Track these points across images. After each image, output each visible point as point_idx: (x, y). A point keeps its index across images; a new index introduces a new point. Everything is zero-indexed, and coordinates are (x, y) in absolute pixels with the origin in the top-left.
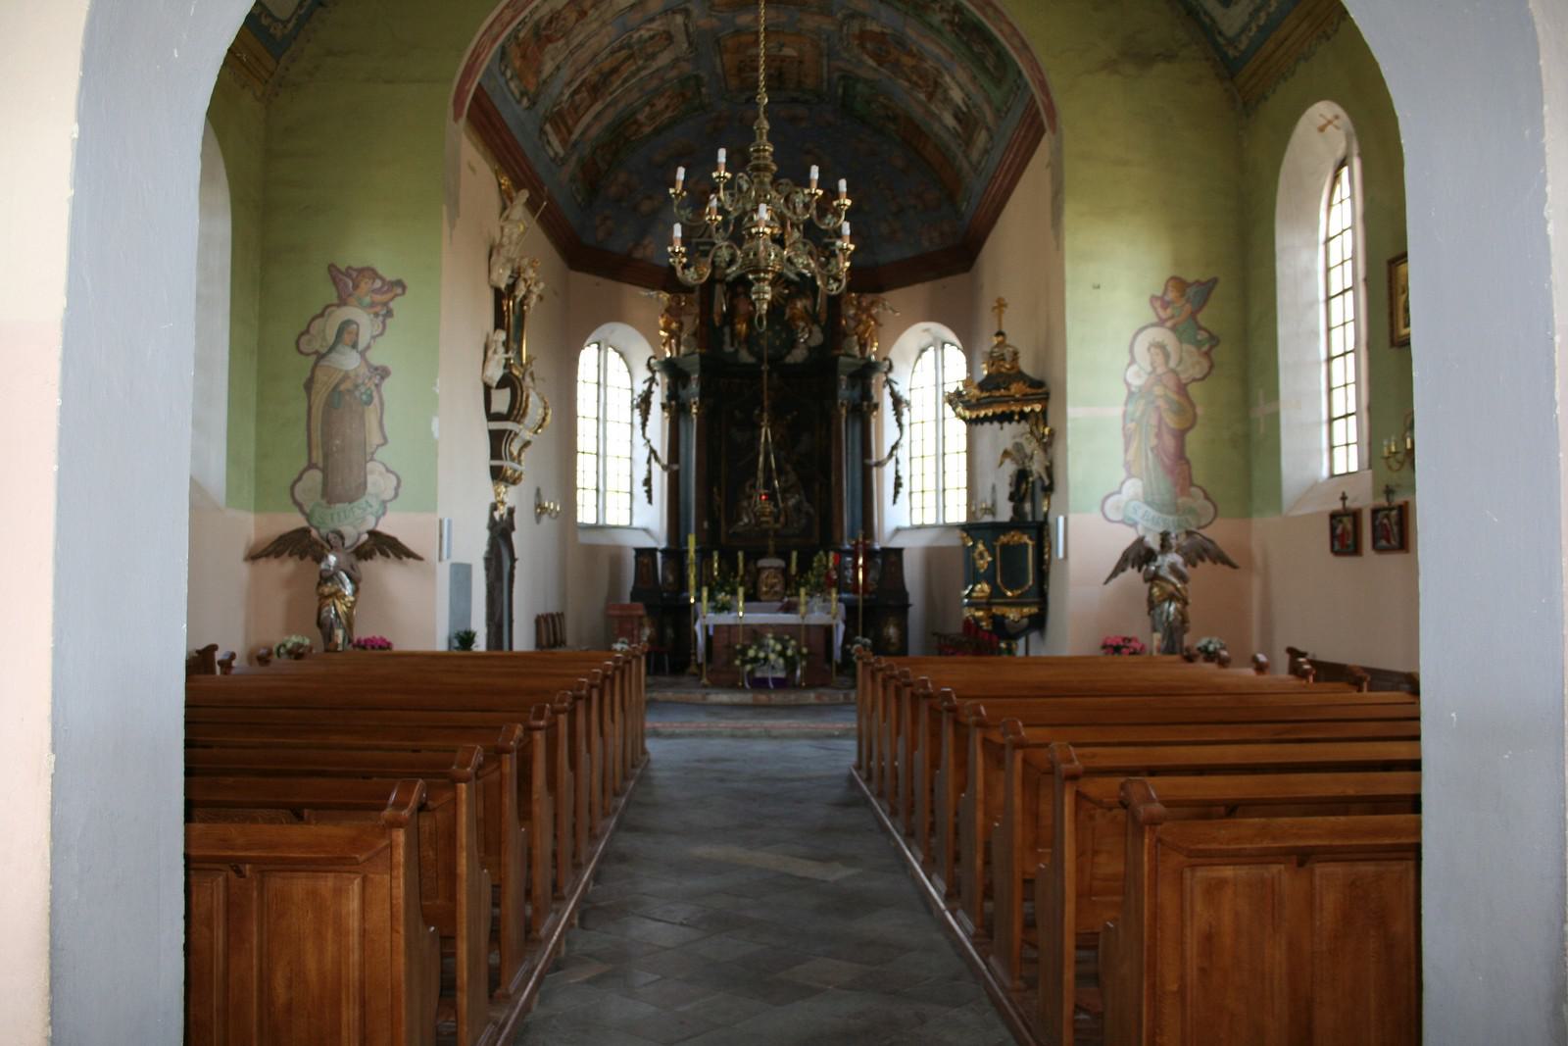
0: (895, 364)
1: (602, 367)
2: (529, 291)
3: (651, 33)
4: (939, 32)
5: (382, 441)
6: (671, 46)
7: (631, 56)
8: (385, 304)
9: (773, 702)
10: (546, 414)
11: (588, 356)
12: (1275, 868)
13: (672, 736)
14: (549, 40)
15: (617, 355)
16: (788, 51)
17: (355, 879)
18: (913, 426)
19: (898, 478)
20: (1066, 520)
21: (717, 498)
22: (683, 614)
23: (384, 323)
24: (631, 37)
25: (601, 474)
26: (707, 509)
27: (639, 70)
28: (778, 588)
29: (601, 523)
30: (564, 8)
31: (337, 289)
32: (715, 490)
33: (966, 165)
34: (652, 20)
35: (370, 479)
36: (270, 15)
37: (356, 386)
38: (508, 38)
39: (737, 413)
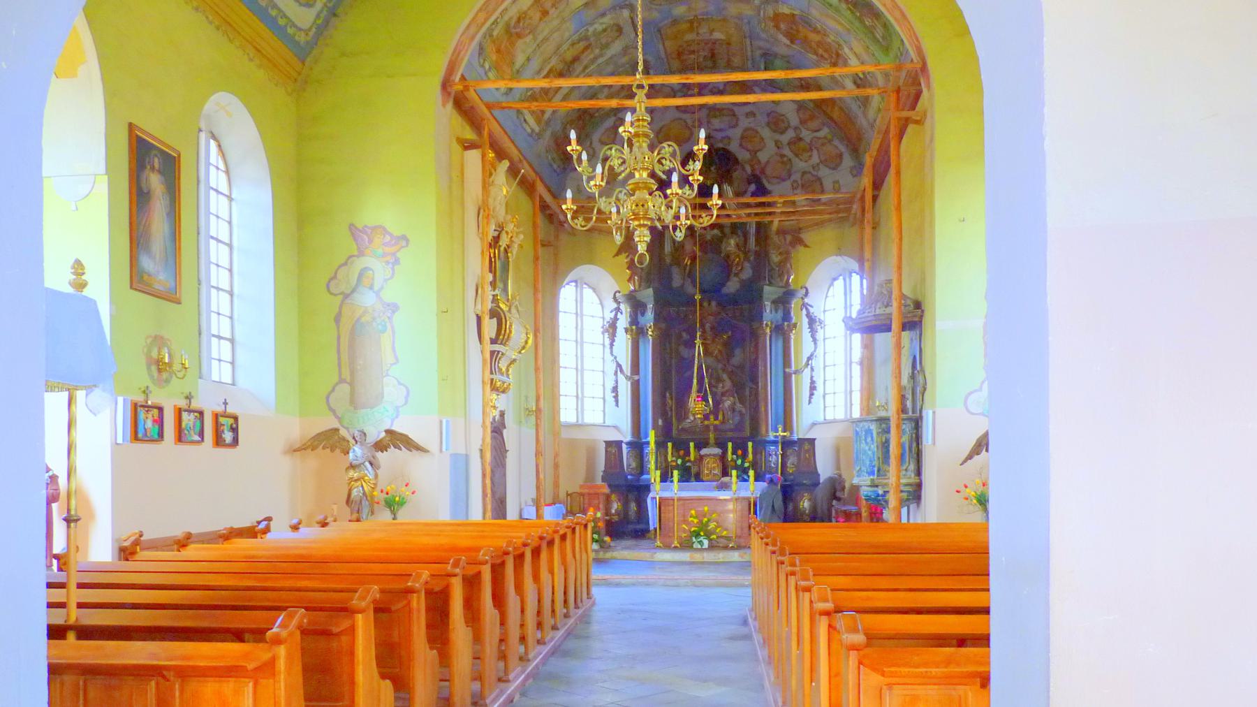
0: (810, 291)
1: (579, 301)
2: (512, 241)
3: (604, 26)
4: (837, 10)
5: (395, 361)
6: (621, 37)
7: (587, 48)
8: (394, 254)
9: (705, 560)
10: (528, 338)
11: (567, 294)
12: (961, 689)
13: (618, 585)
14: (519, 36)
15: (591, 291)
16: (717, 35)
17: (249, 682)
18: (826, 340)
19: (813, 382)
20: (934, 413)
21: (670, 401)
22: (642, 490)
23: (393, 269)
24: (587, 30)
25: (580, 385)
26: (661, 410)
27: (596, 58)
28: (716, 472)
29: (580, 422)
30: (529, 9)
31: (357, 244)
32: (668, 394)
33: (864, 123)
34: (603, 15)
35: (386, 390)
36: (294, 25)
37: (374, 319)
38: (485, 34)
39: (684, 334)
